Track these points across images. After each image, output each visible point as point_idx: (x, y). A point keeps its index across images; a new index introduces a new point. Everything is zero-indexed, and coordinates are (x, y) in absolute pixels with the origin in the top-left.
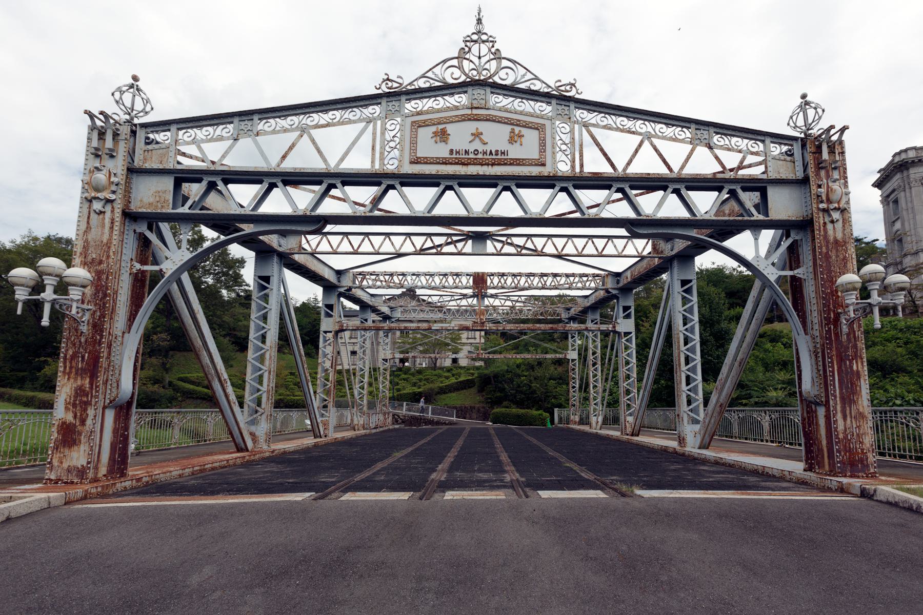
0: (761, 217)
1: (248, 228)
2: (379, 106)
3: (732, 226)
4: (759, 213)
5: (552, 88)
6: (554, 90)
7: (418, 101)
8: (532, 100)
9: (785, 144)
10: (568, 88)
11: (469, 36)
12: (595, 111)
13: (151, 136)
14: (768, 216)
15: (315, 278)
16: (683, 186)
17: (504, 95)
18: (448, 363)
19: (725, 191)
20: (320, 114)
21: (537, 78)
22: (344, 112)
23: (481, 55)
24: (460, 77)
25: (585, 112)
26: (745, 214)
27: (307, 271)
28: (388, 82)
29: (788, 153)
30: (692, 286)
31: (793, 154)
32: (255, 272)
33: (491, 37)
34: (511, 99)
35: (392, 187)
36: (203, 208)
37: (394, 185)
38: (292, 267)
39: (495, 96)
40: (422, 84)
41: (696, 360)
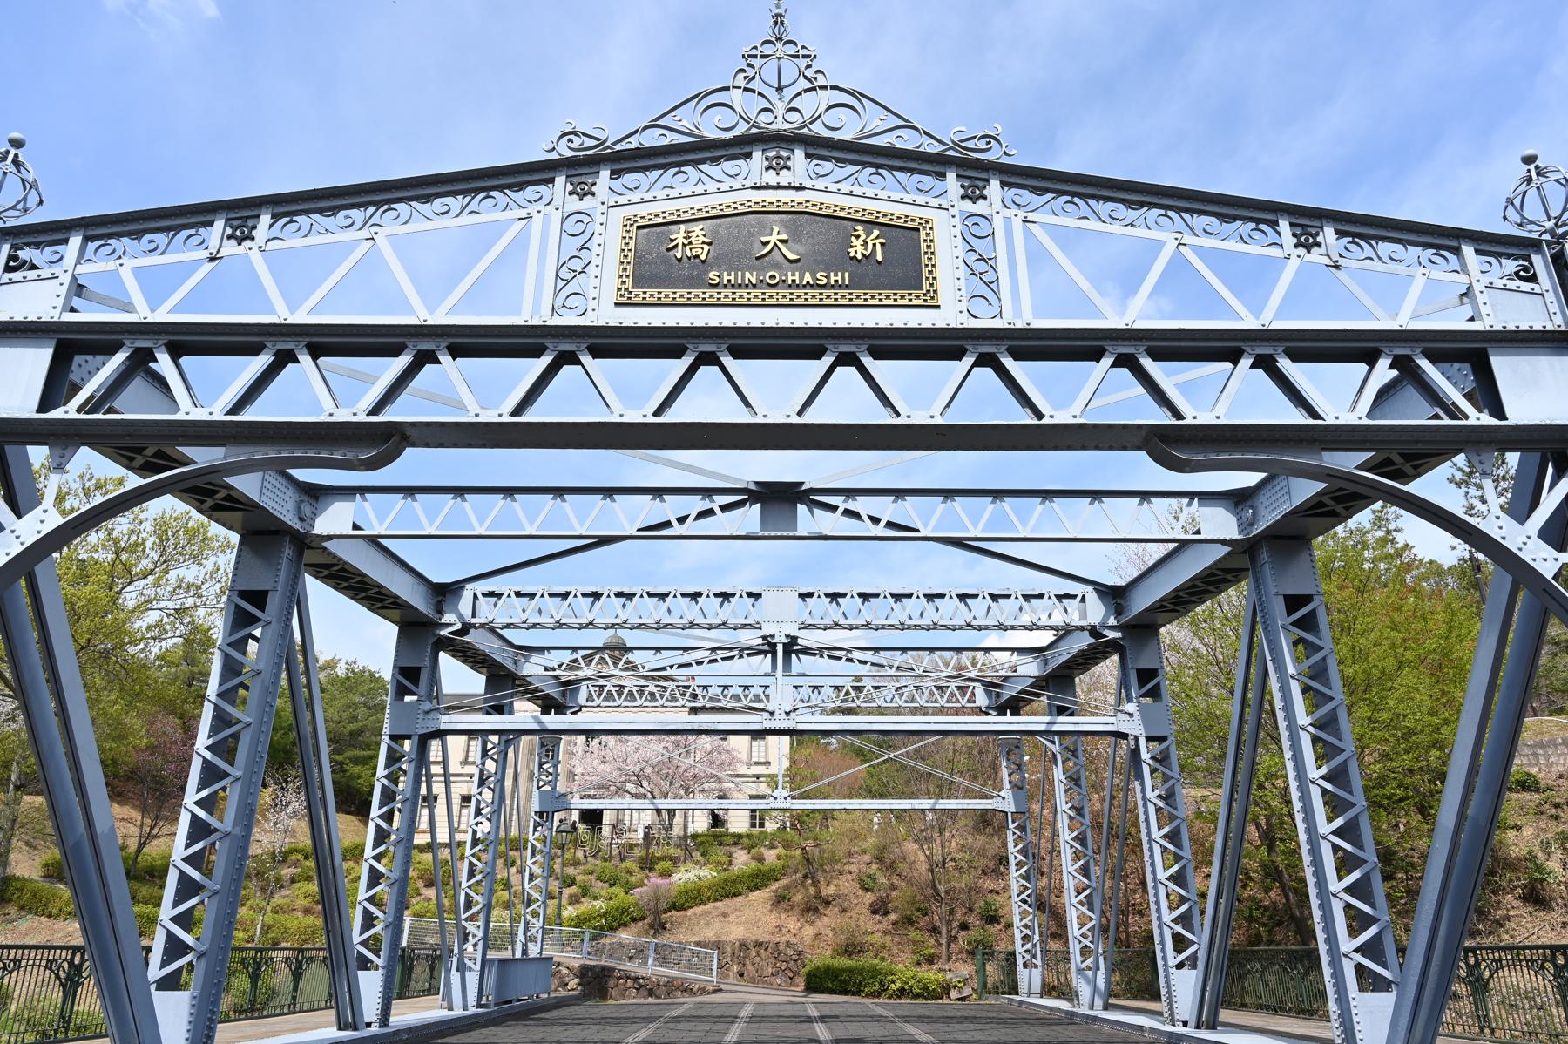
0: (1487, 420)
1: (203, 456)
2: (550, 185)
3: (1417, 442)
4: (1480, 411)
5: (945, 144)
6: (951, 148)
7: (639, 175)
8: (900, 169)
9: (1508, 256)
10: (982, 145)
11: (755, 48)
12: (1047, 191)
13: (24, 254)
14: (1502, 416)
15: (381, 601)
16: (1280, 350)
17: (838, 160)
18: (701, 824)
19: (1383, 363)
20: (414, 204)
21: (909, 126)
22: (468, 198)
23: (782, 84)
24: (737, 124)
25: (1025, 192)
26: (1442, 414)
27: (343, 570)
28: (572, 137)
29: (1522, 273)
30: (1314, 611)
31: (1535, 274)
32: (395, 660)
33: (803, 47)
34: (852, 168)
35: (572, 359)
36: (111, 410)
37: (573, 353)
38: (326, 572)
39: (815, 162)
40: (652, 139)
41: (1353, 805)
